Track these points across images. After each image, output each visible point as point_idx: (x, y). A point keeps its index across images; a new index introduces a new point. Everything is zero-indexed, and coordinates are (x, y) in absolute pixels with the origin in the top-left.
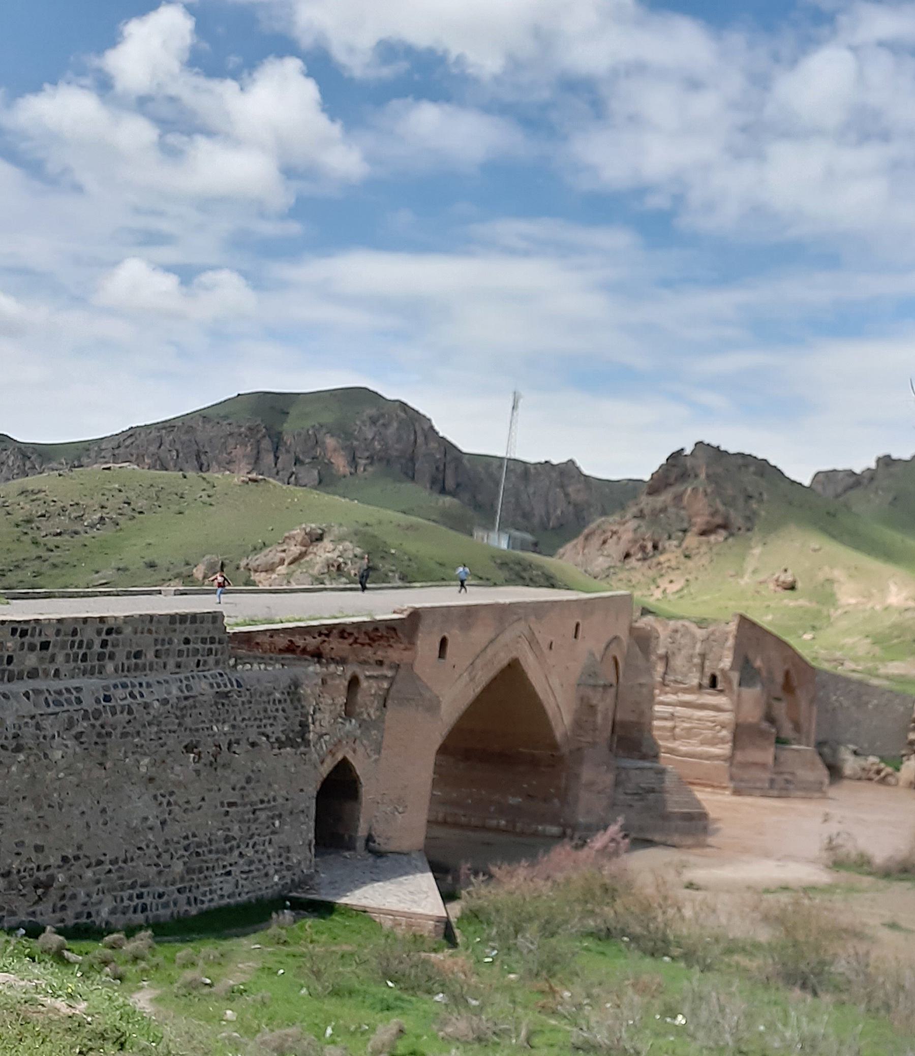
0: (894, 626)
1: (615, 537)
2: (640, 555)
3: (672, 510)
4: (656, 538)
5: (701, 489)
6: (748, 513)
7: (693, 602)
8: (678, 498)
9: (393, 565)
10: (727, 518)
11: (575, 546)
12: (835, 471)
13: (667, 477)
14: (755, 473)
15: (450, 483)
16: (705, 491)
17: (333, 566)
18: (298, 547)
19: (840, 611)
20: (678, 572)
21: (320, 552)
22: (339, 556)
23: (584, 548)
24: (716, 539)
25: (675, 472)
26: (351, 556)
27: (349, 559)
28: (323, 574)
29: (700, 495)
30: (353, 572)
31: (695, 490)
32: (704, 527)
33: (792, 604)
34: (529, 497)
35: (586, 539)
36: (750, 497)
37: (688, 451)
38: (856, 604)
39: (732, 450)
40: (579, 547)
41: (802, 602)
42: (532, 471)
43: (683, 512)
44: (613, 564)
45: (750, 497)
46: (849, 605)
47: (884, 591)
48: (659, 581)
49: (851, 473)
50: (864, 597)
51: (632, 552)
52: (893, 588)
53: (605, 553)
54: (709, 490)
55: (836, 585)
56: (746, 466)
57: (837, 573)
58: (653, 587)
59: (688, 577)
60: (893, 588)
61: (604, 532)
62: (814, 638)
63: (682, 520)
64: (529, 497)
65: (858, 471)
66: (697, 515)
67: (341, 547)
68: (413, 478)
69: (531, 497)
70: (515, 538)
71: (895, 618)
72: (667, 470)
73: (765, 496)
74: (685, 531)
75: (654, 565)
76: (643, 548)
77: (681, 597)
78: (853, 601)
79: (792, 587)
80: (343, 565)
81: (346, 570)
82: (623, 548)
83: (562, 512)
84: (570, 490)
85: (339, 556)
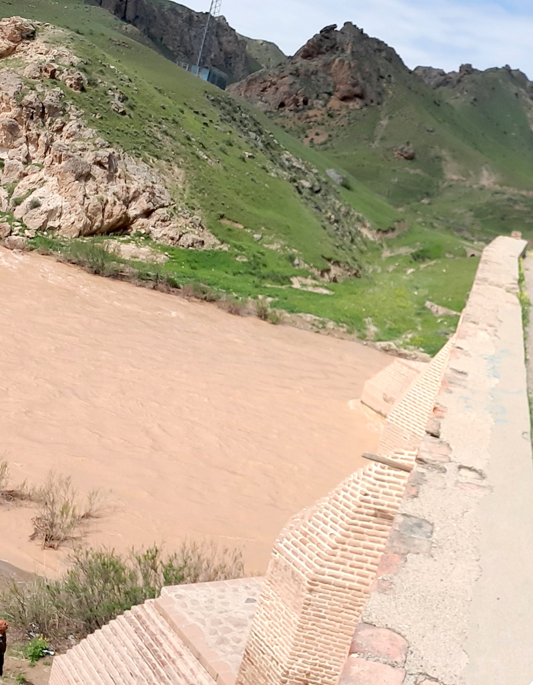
0: (488, 204)
1: (273, 87)
2: (292, 107)
3: (321, 74)
4: (308, 96)
5: (346, 62)
6: (379, 90)
7: (336, 155)
8: (327, 65)
9: (113, 83)
10: (363, 91)
11: (238, 88)
12: (430, 68)
13: (320, 46)
14: (386, 58)
15: (130, 14)
16: (349, 64)
17: (46, 70)
18: (7, 42)
19: (446, 184)
20: (323, 127)
21: (30, 52)
22: (53, 61)
23: (246, 91)
24: (353, 106)
25: (327, 44)
26: (66, 63)
27: (65, 66)
28: (34, 78)
29: (346, 67)
30: (68, 82)
31: (342, 61)
32: (346, 94)
33: (412, 172)
34: (190, 38)
35: (249, 83)
36: (382, 77)
37: (338, 29)
38: (458, 181)
39: (371, 36)
40: (243, 89)
41: (418, 171)
42: (196, 18)
43: (329, 79)
44: (269, 110)
45: (382, 77)
46: (452, 180)
47: (478, 173)
48: (308, 132)
49: (442, 73)
50: (464, 176)
51: (286, 102)
52: (485, 173)
53: (263, 99)
54: (352, 65)
55: (444, 162)
56: (380, 51)
57: (444, 153)
58: (303, 136)
59: (331, 133)
60: (485, 173)
61: (265, 81)
62: (429, 204)
63: (329, 85)
64: (190, 38)
65: (447, 72)
66: (340, 83)
67: (55, 51)
68: (101, 4)
69: (192, 39)
70: (214, 76)
71: (487, 198)
72: (321, 40)
73: (393, 79)
74: (330, 94)
75: (304, 117)
76: (296, 101)
77: (326, 149)
78: (455, 177)
79: (411, 158)
80: (58, 72)
81: (60, 78)
82: (279, 97)
83: (215, 56)
84: (223, 39)
85: (53, 61)
